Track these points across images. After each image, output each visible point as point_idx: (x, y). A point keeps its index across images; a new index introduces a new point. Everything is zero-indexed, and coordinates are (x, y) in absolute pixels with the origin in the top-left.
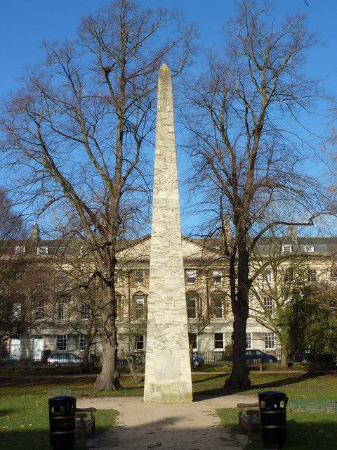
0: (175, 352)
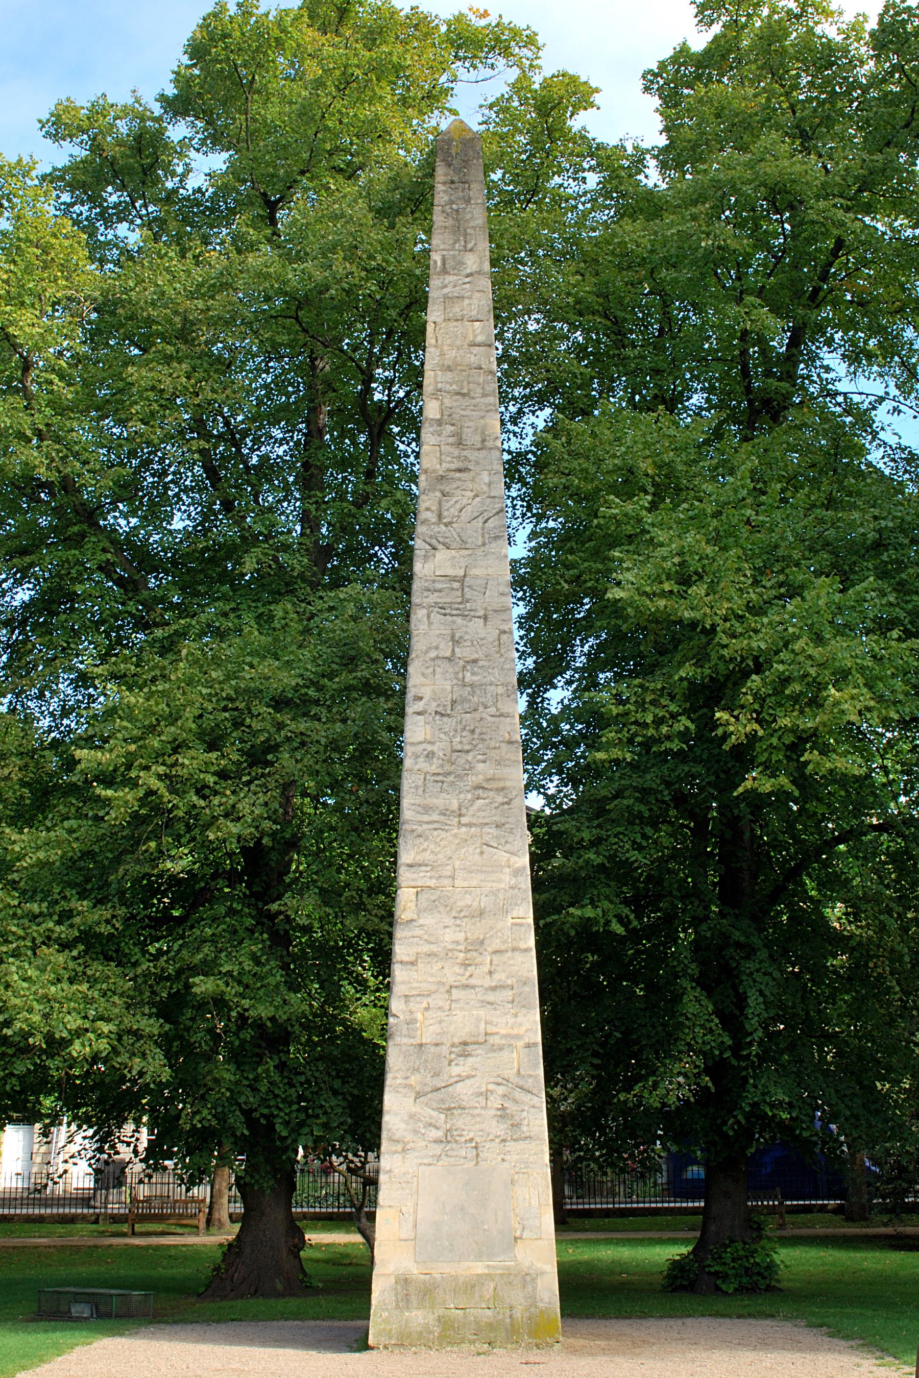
0: (491, 1152)
